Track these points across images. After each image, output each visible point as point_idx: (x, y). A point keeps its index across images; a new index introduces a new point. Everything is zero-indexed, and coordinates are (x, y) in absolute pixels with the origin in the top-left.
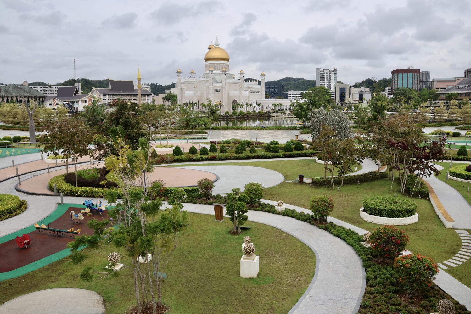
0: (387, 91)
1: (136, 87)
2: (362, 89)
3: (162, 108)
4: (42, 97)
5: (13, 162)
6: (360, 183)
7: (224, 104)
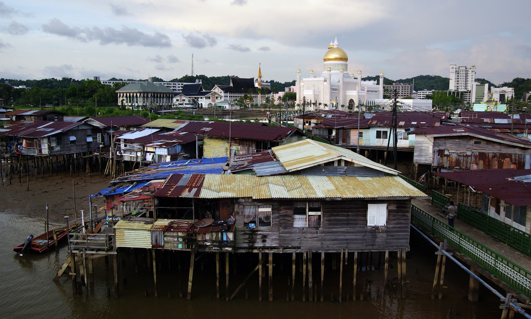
1: (256, 85)
2: (505, 88)
4: (172, 94)
6: (92, 171)
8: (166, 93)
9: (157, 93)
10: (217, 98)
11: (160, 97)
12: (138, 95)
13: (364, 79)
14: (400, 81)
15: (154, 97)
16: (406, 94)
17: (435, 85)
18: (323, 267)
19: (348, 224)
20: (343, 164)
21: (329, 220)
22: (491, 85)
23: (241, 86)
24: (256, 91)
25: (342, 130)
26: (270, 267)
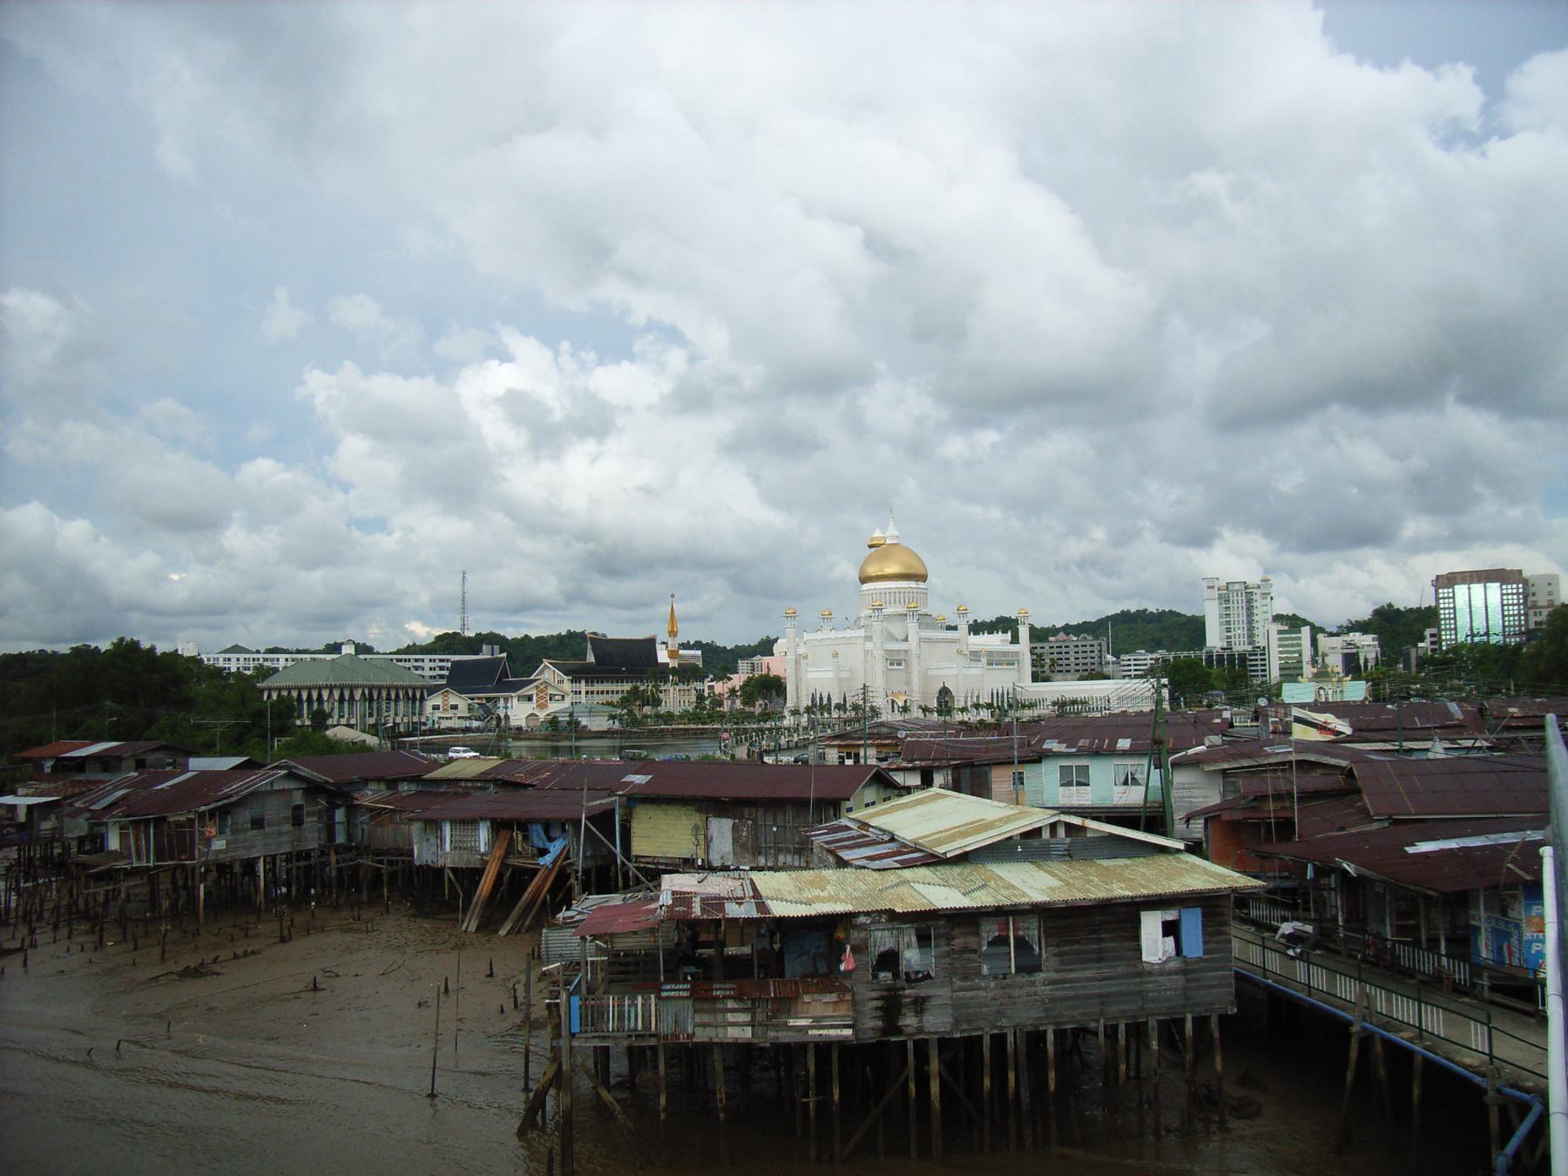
0: (1428, 640)
1: (663, 657)
2: (1356, 637)
4: (422, 688)
5: (25, 964)
8: (406, 688)
9: (380, 688)
11: (388, 698)
12: (325, 694)
13: (976, 628)
14: (1067, 629)
15: (371, 700)
16: (1089, 667)
17: (1160, 635)
18: (1052, 1075)
19: (1100, 960)
20: (1061, 832)
21: (1059, 955)
22: (1316, 630)
23: (625, 662)
25: (967, 771)
26: (935, 1088)
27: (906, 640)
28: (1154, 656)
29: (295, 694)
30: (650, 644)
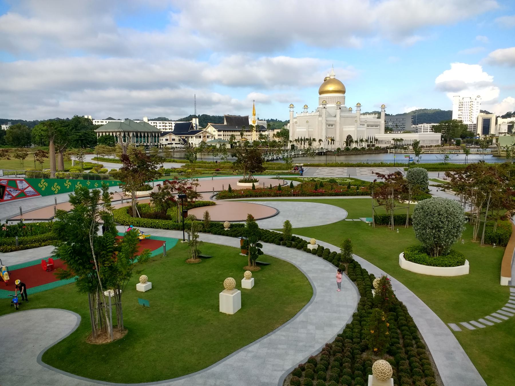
1: (251, 123)
3: (274, 144)
7: (337, 139)
8: (152, 133)
10: (208, 137)
15: (137, 137)
24: (250, 129)
27: (335, 116)
28: (431, 125)
29: (111, 134)
30: (247, 118)
